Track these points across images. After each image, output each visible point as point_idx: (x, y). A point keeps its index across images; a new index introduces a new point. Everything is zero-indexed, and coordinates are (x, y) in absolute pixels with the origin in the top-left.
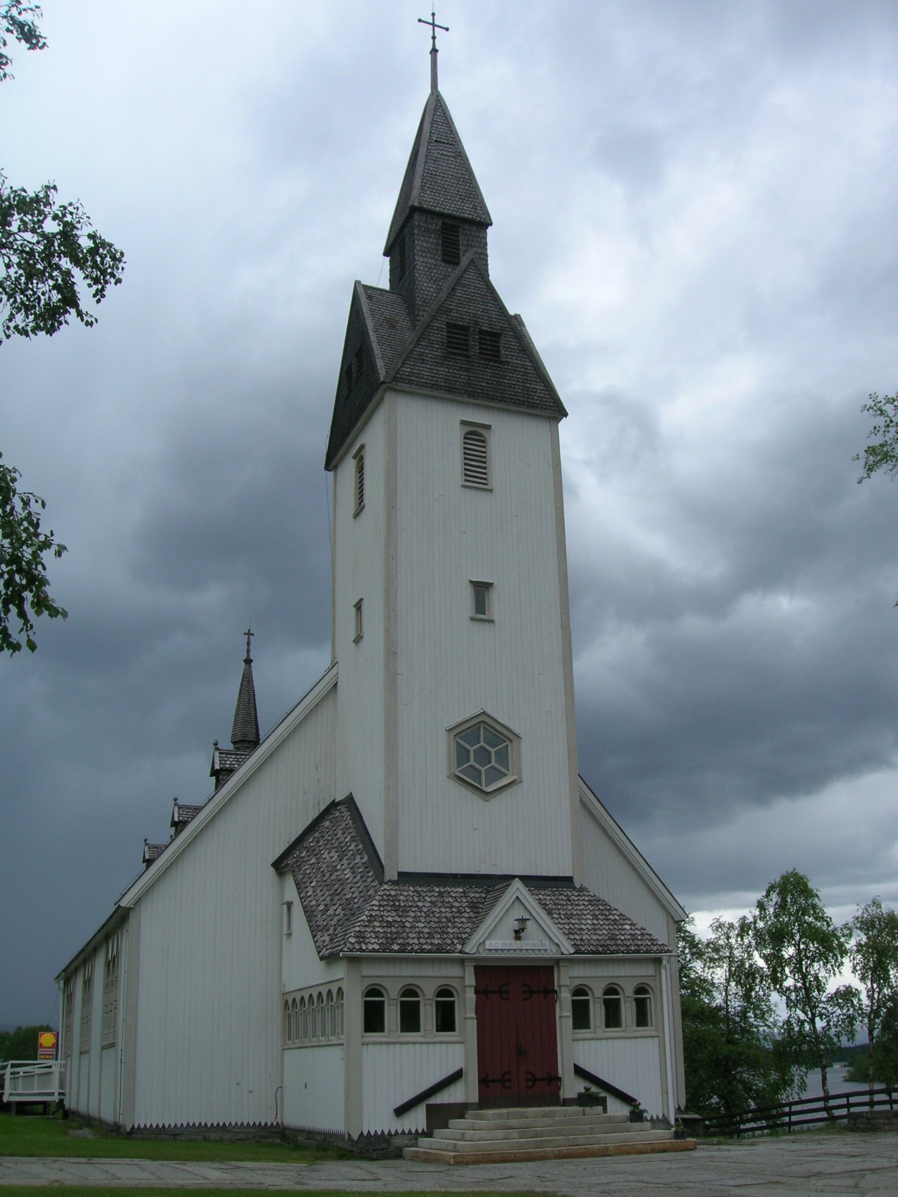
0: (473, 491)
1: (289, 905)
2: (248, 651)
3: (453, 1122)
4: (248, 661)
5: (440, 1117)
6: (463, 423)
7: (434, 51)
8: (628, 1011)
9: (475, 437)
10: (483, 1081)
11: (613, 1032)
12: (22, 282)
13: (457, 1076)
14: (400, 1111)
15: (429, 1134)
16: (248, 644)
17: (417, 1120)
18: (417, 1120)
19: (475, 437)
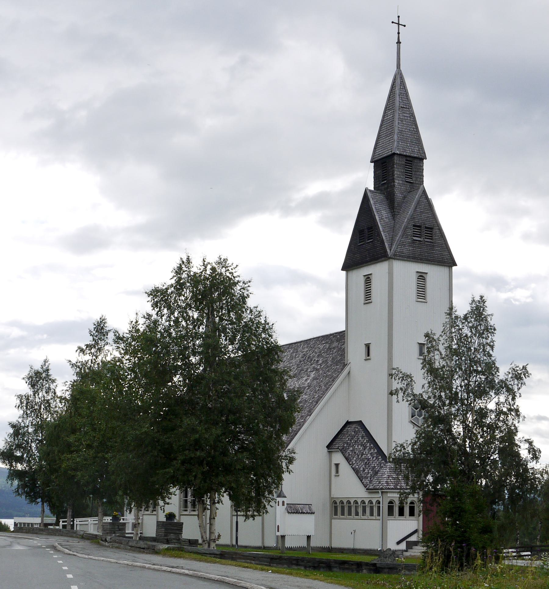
1: (337, 465)
3: (414, 547)
5: (410, 545)
6: (417, 272)
7: (399, 42)
8: (407, 510)
9: (422, 277)
10: (424, 535)
11: (401, 518)
12: (198, 453)
13: (416, 531)
14: (398, 543)
15: (406, 551)
17: (403, 546)
18: (403, 546)
19: (422, 277)
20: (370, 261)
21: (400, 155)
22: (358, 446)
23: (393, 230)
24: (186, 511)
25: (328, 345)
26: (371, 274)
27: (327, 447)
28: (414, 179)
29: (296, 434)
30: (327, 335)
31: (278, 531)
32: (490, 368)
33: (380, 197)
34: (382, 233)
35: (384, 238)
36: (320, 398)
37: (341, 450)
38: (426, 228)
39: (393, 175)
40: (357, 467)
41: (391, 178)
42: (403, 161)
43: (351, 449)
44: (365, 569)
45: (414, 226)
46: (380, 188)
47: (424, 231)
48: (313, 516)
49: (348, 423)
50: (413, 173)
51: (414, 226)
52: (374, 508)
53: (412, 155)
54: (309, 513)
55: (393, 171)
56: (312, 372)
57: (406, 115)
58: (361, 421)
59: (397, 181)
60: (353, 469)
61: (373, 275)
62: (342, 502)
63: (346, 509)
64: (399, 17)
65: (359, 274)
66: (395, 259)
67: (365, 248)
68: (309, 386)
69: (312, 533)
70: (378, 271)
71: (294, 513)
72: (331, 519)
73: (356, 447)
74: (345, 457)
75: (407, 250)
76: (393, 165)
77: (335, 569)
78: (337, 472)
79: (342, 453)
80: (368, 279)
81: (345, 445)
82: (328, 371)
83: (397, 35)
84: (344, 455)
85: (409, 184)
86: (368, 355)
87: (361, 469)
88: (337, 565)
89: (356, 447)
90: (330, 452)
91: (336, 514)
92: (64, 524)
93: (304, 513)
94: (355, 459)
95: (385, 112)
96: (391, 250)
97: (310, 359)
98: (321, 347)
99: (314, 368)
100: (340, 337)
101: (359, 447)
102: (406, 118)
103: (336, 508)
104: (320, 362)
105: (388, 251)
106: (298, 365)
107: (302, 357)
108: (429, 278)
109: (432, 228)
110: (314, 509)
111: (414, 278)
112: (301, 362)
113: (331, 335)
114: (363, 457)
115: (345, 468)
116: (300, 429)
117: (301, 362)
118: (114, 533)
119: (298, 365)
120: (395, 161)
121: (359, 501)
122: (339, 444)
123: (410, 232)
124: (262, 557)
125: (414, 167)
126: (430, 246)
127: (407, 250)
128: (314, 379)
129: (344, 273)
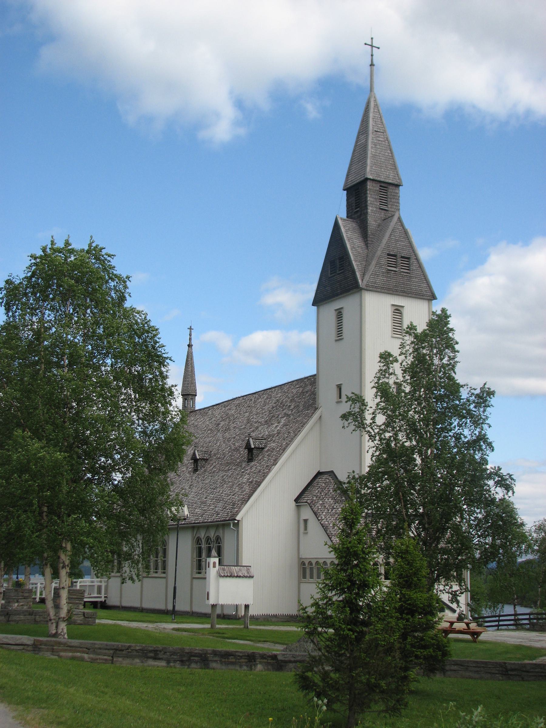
0: (396, 339)
1: (306, 521)
2: (190, 339)
4: (190, 346)
6: (393, 305)
16: (190, 335)
20: (341, 294)
21: (373, 180)
22: (328, 499)
23: (367, 261)
24: (156, 572)
25: (301, 389)
26: (342, 308)
27: (295, 500)
28: (389, 206)
29: (259, 486)
30: (302, 379)
31: (208, 599)
32: (454, 388)
33: (352, 225)
34: (353, 262)
35: (356, 267)
36: (288, 445)
37: (309, 504)
38: (402, 257)
39: (366, 201)
40: (327, 523)
41: (363, 205)
42: (377, 187)
43: (321, 502)
44: (260, 663)
45: (389, 255)
46: (353, 216)
47: (399, 261)
48: (251, 581)
49: (319, 474)
50: (389, 200)
51: (389, 255)
52: (314, 570)
53: (387, 181)
54: (246, 577)
55: (366, 197)
56: (283, 417)
57: (380, 139)
58: (332, 472)
59: (371, 208)
60: (322, 525)
61: (344, 309)
62: (310, 563)
63: (308, 571)
64: (372, 38)
65: (330, 309)
66: (367, 290)
67: (337, 281)
68: (278, 433)
69: (250, 602)
70: (347, 304)
71: (227, 576)
72: (300, 583)
73: (326, 500)
74: (313, 511)
75: (381, 280)
76: (366, 191)
77: (214, 665)
78: (306, 528)
79: (311, 507)
80: (339, 314)
81: (315, 498)
82: (299, 416)
83: (370, 57)
84: (312, 509)
85: (384, 211)
86: (340, 398)
87: (331, 525)
88: (216, 658)
89: (326, 500)
90: (298, 507)
91: (304, 577)
92: (81, 584)
93: (240, 577)
94: (324, 514)
95: (358, 137)
96: (362, 280)
97: (282, 405)
98: (294, 391)
99: (285, 414)
100: (312, 380)
101: (330, 500)
102: (380, 142)
103: (304, 570)
104: (292, 407)
105: (360, 281)
106: (270, 411)
107: (275, 403)
108: (405, 312)
109: (408, 258)
110: (253, 571)
111: (388, 312)
112: (273, 408)
113: (305, 378)
114: (334, 511)
115: (313, 523)
116: (263, 480)
117: (273, 408)
118: (18, 602)
119: (270, 411)
120: (368, 187)
121: (314, 562)
122: (308, 497)
123: (384, 261)
124: (100, 649)
125: (389, 193)
126: (406, 275)
127: (381, 280)
128: (285, 425)
129: (315, 308)
